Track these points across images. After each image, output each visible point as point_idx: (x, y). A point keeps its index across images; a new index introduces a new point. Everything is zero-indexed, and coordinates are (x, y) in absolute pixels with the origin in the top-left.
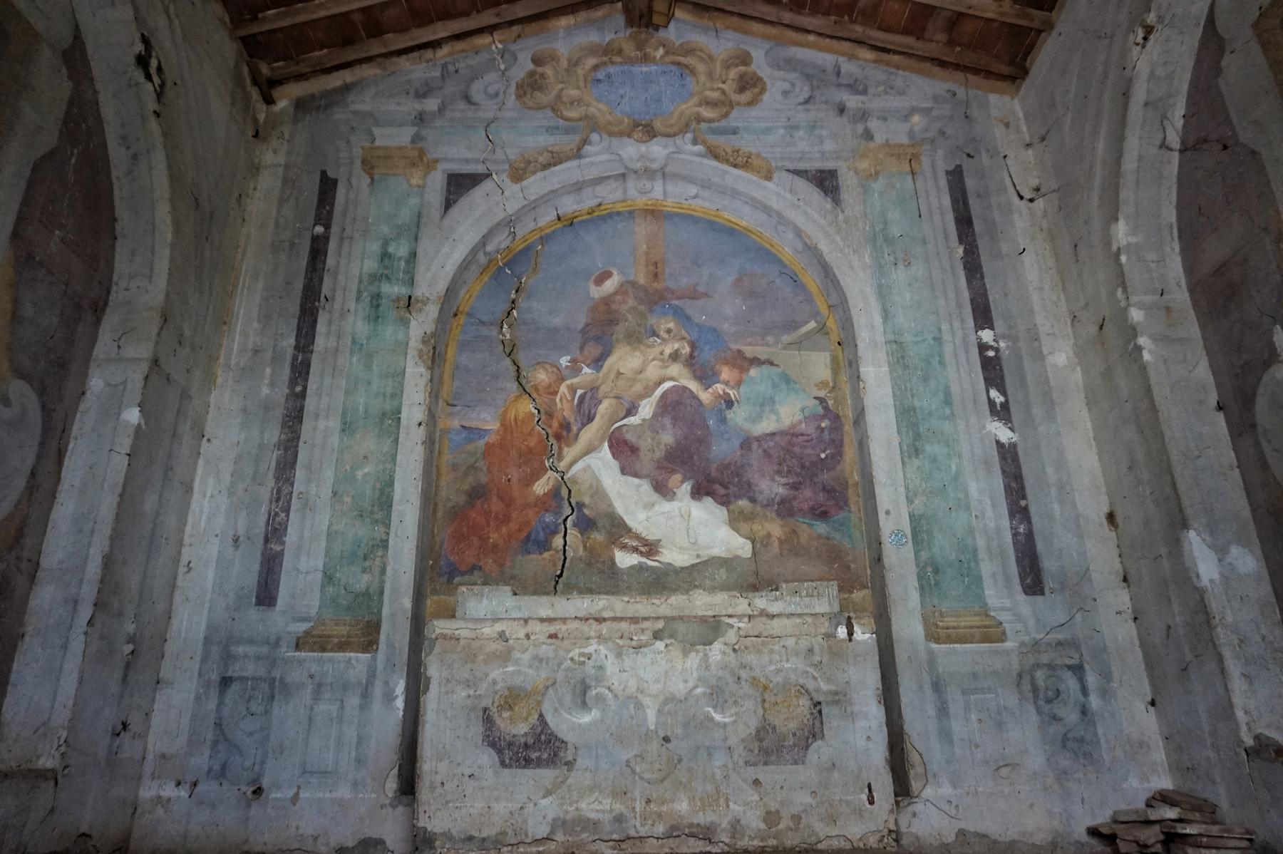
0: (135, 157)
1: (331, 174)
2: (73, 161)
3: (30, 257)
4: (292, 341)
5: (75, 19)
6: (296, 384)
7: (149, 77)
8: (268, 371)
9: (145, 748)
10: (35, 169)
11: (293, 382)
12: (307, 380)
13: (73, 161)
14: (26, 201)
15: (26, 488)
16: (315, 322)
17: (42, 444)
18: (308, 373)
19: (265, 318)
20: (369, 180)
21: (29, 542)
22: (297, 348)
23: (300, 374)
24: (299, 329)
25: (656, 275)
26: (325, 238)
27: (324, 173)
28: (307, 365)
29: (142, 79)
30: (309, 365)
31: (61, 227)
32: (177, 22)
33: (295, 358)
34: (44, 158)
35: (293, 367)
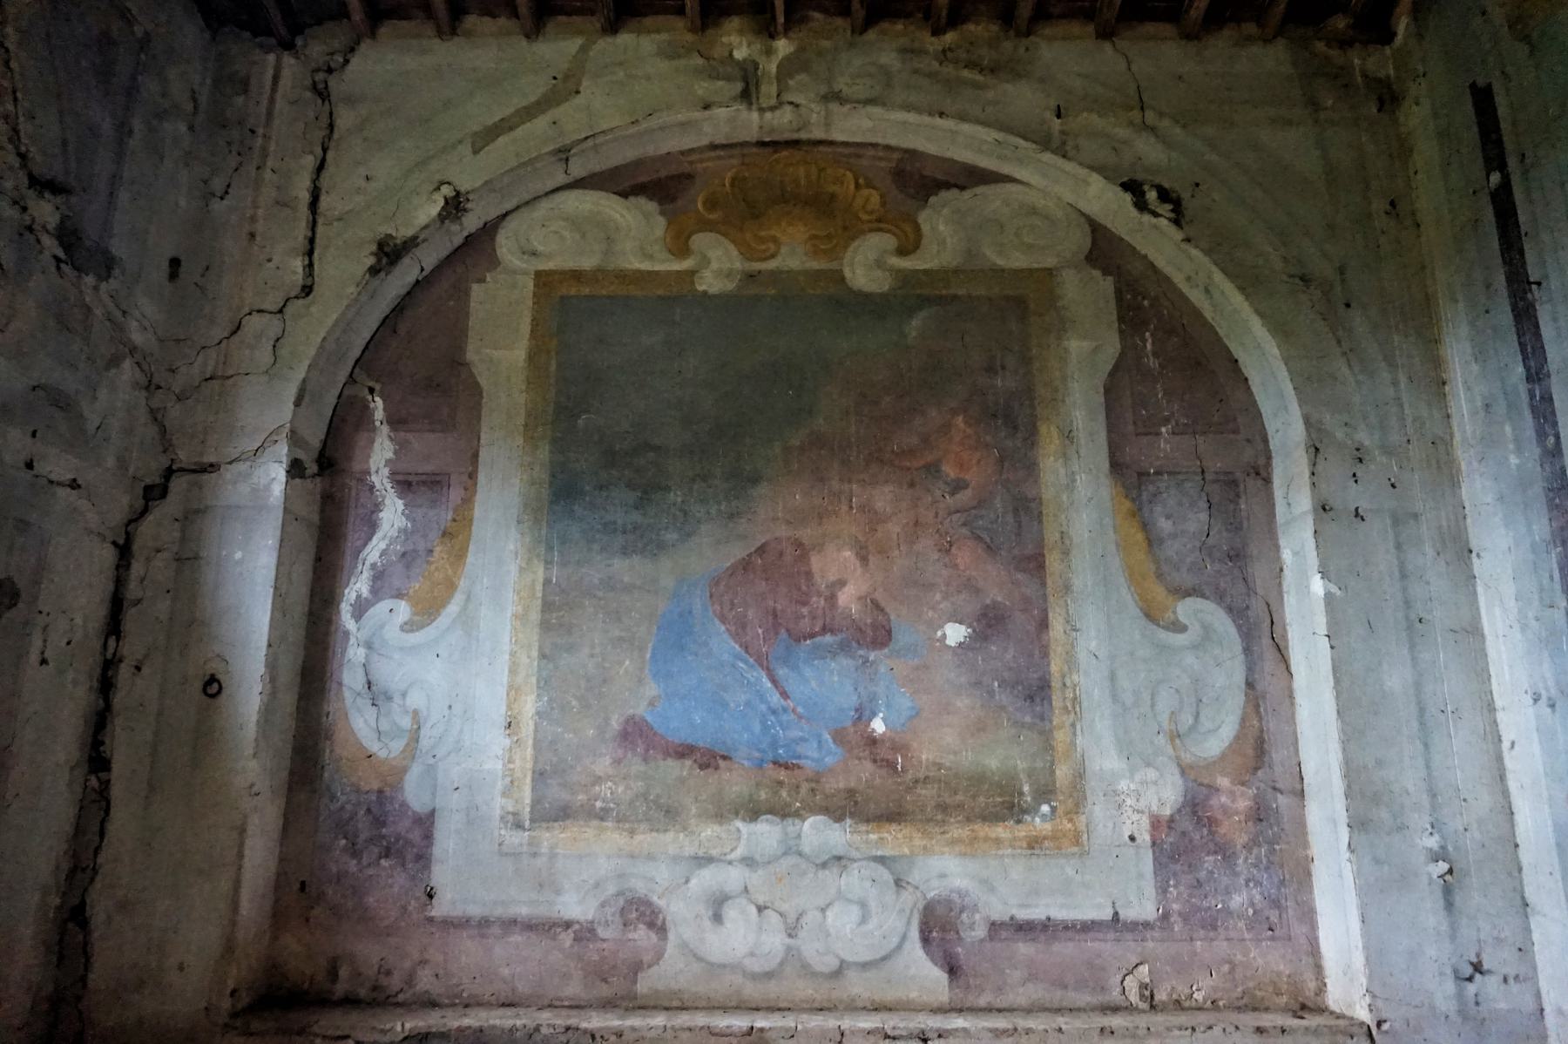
0: (1207, 291)
1: (1481, 82)
2: (1149, 346)
3: (1142, 474)
4: (1520, 369)
5: (1083, 214)
6: (1546, 435)
7: (1156, 215)
8: (1508, 429)
9: (1538, 995)
10: (1107, 391)
11: (1541, 435)
12: (1555, 424)
13: (1149, 346)
14: (1111, 428)
15: (1247, 702)
16: (1537, 326)
17: (1247, 650)
18: (1553, 413)
19: (1480, 355)
20: (1526, 48)
21: (1277, 755)
22: (1529, 379)
23: (1545, 418)
24: (1522, 346)
25: (1305, 280)
26: (1506, 185)
27: (1473, 86)
28: (1548, 399)
29: (1154, 220)
30: (1551, 399)
31: (1166, 421)
32: (1166, 123)
33: (1532, 395)
34: (1112, 374)
35: (1533, 409)
